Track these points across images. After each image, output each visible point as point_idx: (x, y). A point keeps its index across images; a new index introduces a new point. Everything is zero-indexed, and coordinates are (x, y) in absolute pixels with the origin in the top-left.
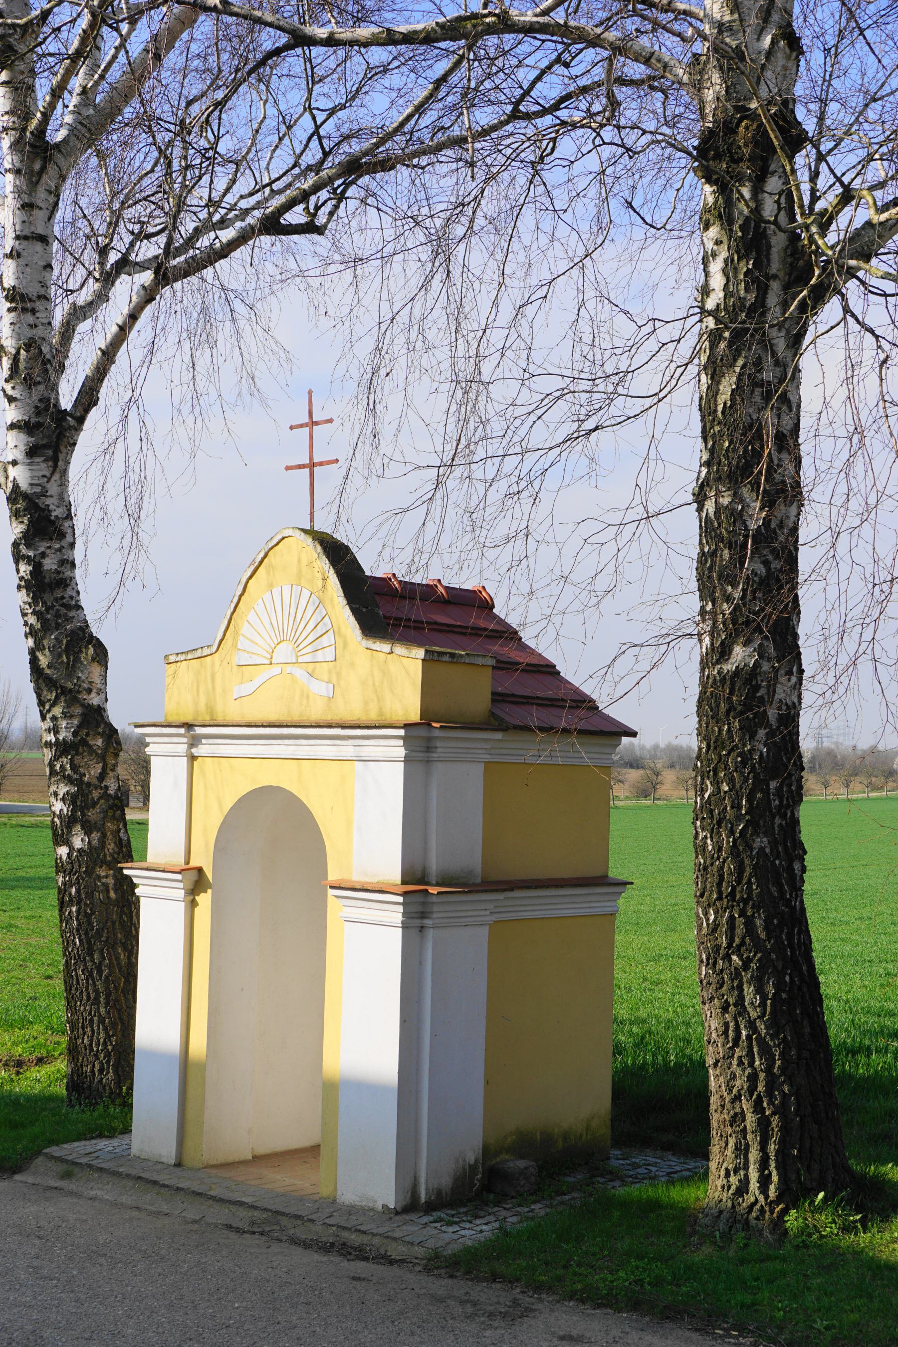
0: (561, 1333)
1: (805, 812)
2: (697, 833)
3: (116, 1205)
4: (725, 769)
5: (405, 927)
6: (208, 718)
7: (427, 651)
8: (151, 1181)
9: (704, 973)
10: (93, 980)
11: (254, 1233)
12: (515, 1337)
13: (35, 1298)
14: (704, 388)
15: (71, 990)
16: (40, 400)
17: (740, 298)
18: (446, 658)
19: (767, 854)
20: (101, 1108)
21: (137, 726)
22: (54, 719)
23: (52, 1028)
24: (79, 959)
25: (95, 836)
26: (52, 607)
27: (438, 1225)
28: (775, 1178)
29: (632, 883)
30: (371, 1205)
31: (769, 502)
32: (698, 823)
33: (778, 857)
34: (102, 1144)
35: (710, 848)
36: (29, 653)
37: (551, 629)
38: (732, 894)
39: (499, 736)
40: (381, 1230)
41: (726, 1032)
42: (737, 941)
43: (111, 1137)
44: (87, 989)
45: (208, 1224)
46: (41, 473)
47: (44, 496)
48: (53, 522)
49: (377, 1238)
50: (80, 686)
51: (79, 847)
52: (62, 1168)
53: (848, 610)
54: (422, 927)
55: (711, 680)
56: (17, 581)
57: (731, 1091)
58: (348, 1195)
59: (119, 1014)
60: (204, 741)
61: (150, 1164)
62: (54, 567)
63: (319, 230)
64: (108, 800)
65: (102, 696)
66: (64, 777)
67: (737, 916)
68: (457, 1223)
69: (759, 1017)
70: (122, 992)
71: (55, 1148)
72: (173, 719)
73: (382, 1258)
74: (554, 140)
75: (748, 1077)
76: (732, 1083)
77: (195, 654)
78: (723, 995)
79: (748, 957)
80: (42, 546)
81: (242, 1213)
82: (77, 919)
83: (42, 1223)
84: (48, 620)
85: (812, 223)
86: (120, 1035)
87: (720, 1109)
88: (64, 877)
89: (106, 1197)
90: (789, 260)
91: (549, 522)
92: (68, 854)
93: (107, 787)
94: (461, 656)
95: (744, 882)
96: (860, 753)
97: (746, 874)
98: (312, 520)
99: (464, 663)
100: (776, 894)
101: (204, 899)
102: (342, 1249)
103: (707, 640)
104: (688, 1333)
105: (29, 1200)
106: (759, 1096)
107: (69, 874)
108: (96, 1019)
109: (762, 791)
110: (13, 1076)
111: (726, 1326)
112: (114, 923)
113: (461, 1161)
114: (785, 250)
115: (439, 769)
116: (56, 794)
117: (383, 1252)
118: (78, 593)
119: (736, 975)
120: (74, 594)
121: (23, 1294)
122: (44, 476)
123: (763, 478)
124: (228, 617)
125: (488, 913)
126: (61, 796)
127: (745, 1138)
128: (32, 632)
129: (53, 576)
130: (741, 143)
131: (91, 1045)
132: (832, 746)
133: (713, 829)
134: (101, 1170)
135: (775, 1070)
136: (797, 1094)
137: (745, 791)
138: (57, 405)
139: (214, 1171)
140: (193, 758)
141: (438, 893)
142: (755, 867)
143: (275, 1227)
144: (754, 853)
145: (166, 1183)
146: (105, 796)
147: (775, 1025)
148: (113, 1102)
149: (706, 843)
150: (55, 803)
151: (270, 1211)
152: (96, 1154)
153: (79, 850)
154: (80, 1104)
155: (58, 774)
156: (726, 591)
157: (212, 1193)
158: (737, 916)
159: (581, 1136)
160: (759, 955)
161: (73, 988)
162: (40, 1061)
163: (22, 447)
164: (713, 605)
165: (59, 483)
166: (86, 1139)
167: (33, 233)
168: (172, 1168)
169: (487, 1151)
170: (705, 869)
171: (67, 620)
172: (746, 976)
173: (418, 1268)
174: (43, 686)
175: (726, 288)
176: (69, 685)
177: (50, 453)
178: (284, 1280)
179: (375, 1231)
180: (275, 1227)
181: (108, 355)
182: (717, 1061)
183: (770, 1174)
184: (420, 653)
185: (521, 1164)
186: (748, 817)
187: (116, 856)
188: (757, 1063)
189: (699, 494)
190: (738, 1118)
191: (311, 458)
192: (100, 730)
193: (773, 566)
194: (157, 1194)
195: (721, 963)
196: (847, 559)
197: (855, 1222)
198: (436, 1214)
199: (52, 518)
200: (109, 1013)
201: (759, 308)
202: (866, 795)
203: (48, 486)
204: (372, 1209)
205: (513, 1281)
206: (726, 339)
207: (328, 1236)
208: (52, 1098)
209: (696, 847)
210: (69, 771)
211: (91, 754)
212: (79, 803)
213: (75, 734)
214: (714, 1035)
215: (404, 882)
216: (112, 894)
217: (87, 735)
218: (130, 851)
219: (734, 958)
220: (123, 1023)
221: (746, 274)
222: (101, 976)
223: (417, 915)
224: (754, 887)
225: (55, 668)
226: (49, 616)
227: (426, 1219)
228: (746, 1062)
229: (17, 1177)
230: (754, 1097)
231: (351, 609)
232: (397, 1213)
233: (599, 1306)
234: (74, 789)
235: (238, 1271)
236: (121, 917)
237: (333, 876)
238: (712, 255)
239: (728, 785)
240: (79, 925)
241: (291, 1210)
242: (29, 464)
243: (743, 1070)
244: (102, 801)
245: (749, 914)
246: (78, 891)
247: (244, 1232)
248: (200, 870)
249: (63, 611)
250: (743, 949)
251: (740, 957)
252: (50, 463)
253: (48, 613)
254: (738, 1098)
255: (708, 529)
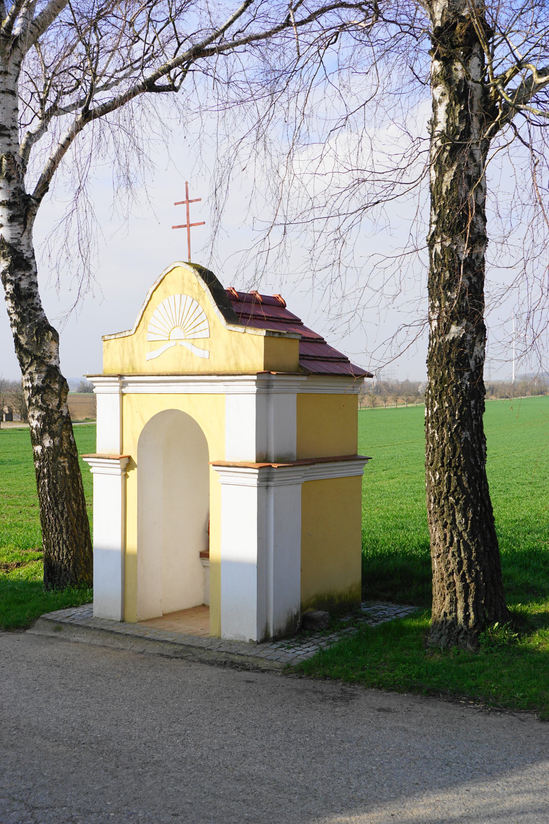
0: (377, 707)
1: (486, 418)
2: (428, 430)
3: (92, 645)
4: (446, 394)
5: (259, 487)
6: (131, 371)
7: (267, 331)
8: (109, 631)
9: (432, 507)
10: (59, 520)
11: (177, 658)
12: (353, 711)
13: (73, 702)
14: (434, 179)
15: (45, 526)
16: (15, 189)
17: (456, 127)
18: (277, 335)
19: (469, 441)
20: (66, 590)
21: (88, 377)
22: (31, 373)
23: (19, 546)
24: (50, 508)
25: (57, 439)
26: (27, 309)
27: (283, 649)
28: (472, 616)
29: (371, 458)
30: (242, 639)
31: (472, 243)
32: (430, 425)
33: (474, 443)
34: (73, 611)
35: (437, 438)
36: (14, 336)
37: (357, 318)
38: (450, 464)
39: (305, 378)
40: (252, 653)
41: (445, 539)
42: (452, 489)
43: (76, 607)
44: (55, 525)
45: (148, 654)
46: (17, 232)
47: (19, 245)
48: (25, 260)
49: (251, 658)
50: (45, 354)
51: (48, 446)
52: (54, 625)
53: (532, 304)
54: (267, 486)
55: (437, 345)
56: (5, 295)
57: (447, 570)
58: (228, 634)
59: (74, 538)
60: (129, 384)
61: (106, 621)
62: (27, 286)
63: (176, 89)
64: (63, 419)
65: (57, 360)
66: (38, 406)
67: (452, 475)
68: (292, 647)
69: (464, 530)
70: (75, 526)
71: (47, 614)
72: (109, 372)
73: (257, 669)
74: (337, 34)
75: (458, 563)
76: (448, 566)
77: (120, 335)
78: (444, 519)
79: (458, 498)
80: (19, 274)
81: (167, 647)
82: (48, 486)
83: (55, 658)
84: (24, 317)
85: (498, 83)
86: (75, 550)
87: (440, 580)
88: (40, 463)
89: (85, 641)
90: (483, 105)
91: (351, 256)
92: (42, 450)
93: (62, 412)
94: (284, 334)
95: (456, 456)
96: (401, 384)
97: (458, 452)
98: (189, 257)
99: (286, 338)
100: (473, 463)
101: (133, 474)
102: (232, 665)
103: (435, 323)
104: (445, 703)
105: (41, 644)
106: (464, 573)
107: (43, 461)
108: (61, 542)
109: (467, 406)
110: (5, 574)
111: (464, 698)
112: (69, 488)
113: (290, 613)
114: (481, 99)
115: (274, 397)
116: (33, 416)
117: (256, 665)
118: (40, 301)
119: (452, 507)
120: (38, 302)
121: (65, 700)
122: (19, 233)
123: (468, 231)
124: (141, 313)
125: (301, 477)
126: (36, 417)
127: (455, 595)
128: (15, 324)
129: (26, 291)
130: (458, 36)
131: (59, 556)
132: (386, 380)
133: (439, 428)
134: (78, 626)
135: (473, 558)
136: (483, 571)
137: (458, 407)
138: (23, 192)
139: (144, 624)
140: (123, 394)
141: (278, 467)
142: (463, 448)
143: (189, 654)
144: (462, 441)
145: (119, 631)
146: (61, 416)
147: (472, 534)
148: (73, 587)
149: (434, 436)
150: (33, 421)
151: (185, 645)
152: (72, 617)
153: (48, 448)
154: (54, 589)
155: (33, 405)
156: (447, 295)
157: (147, 636)
158: (452, 475)
159: (347, 596)
160: (464, 496)
161: (47, 525)
162: (18, 565)
163: (6, 217)
164: (440, 303)
165: (27, 237)
166: (63, 609)
167: (7, 89)
168: (119, 623)
169: (303, 608)
170: (434, 450)
171: (35, 317)
172: (457, 508)
173: (280, 674)
174: (23, 355)
175: (447, 121)
176: (39, 354)
177: (22, 219)
178: (209, 684)
179: (249, 654)
180: (189, 654)
181: (54, 163)
182: (440, 555)
183: (469, 614)
185: (321, 613)
186: (459, 421)
187: (68, 450)
188: (463, 555)
189: (431, 240)
190: (451, 585)
191: (188, 221)
192: (57, 379)
193: (473, 280)
194: (114, 638)
195: (443, 501)
196: (532, 276)
197: (516, 637)
198: (280, 643)
199: (25, 258)
200: (68, 538)
201: (467, 134)
202: (405, 406)
203: (21, 239)
204: (243, 642)
205: (336, 679)
206: (447, 150)
207: (222, 658)
208: (35, 585)
209: (427, 437)
210: (40, 403)
211: (52, 393)
212: (47, 421)
213: (43, 382)
214: (438, 541)
215: (257, 462)
216: (68, 472)
217: (50, 382)
218: (76, 448)
219: (451, 498)
220: (76, 543)
221: (459, 113)
222: (63, 517)
223: (265, 480)
224: (462, 459)
225: (30, 345)
226: (25, 315)
227: (275, 646)
228: (456, 555)
229: (28, 631)
230: (461, 573)
231: (219, 308)
232: (258, 643)
233: (390, 690)
234: (44, 413)
235: (180, 681)
236: (73, 485)
237: (213, 459)
238: (439, 102)
239: (448, 403)
240: (49, 489)
241: (196, 644)
242: (10, 226)
243: (455, 559)
244: (60, 420)
245: (459, 474)
246: (48, 471)
247: (172, 658)
248: (129, 458)
249: (33, 311)
250: (455, 493)
251: (454, 497)
252: (22, 226)
253: (24, 313)
254: (452, 574)
255: (435, 260)
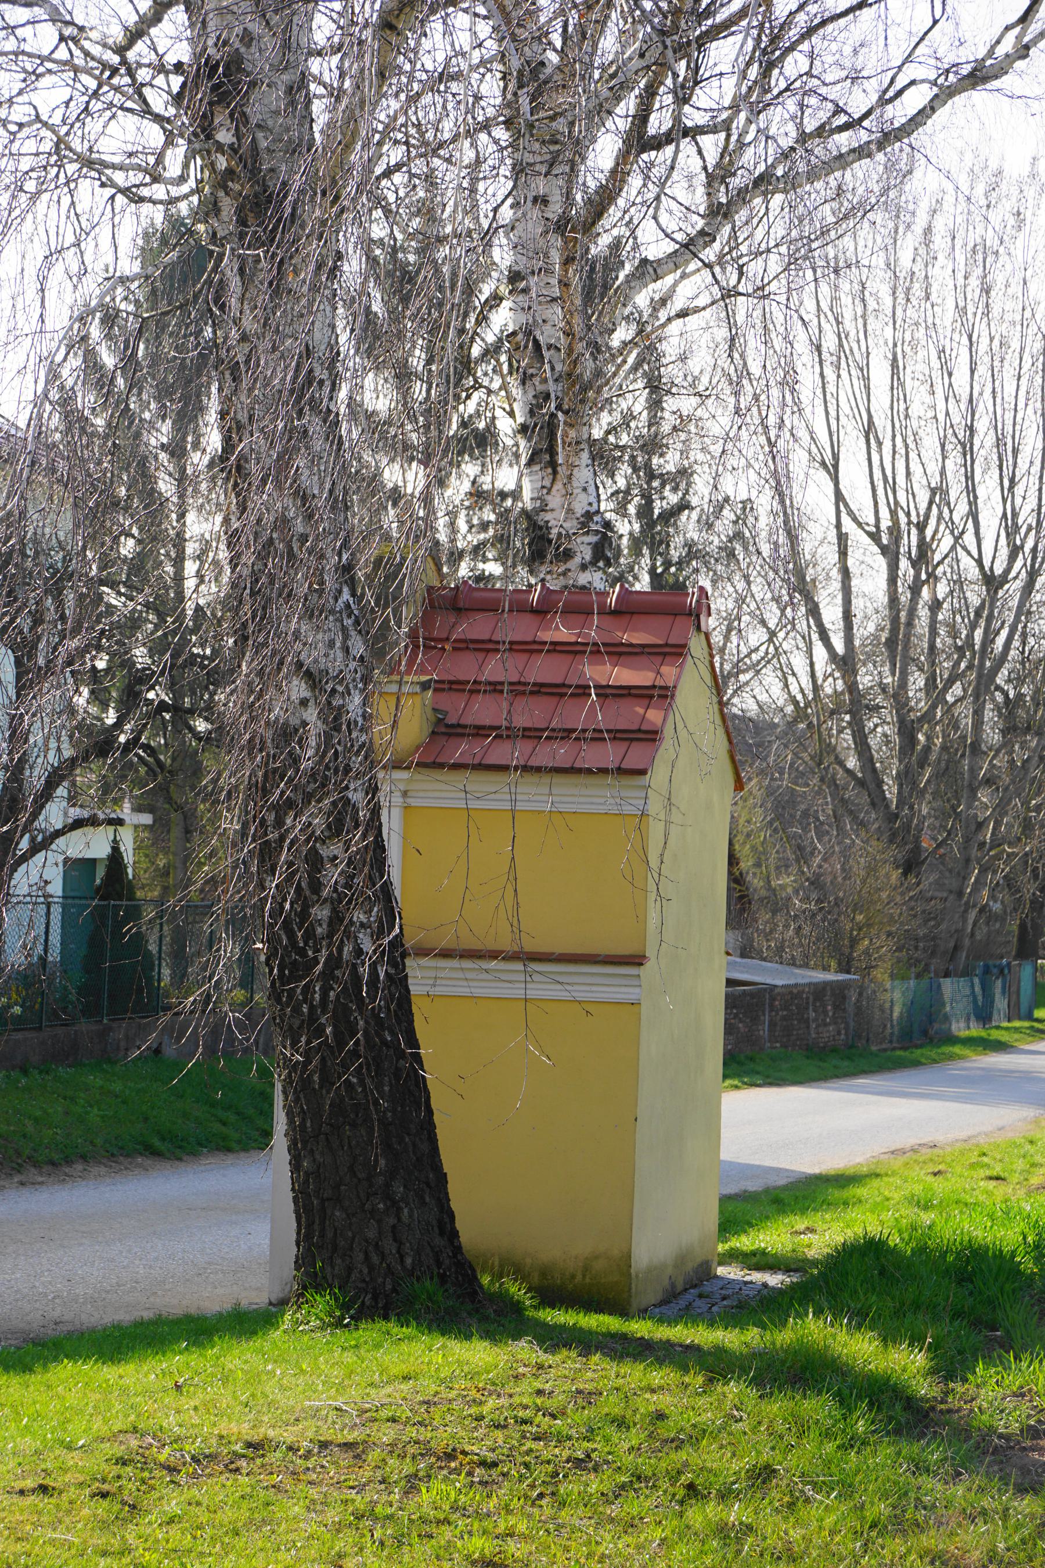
159: (573, 1277)
184: (724, 1156)
203: (549, 498)
